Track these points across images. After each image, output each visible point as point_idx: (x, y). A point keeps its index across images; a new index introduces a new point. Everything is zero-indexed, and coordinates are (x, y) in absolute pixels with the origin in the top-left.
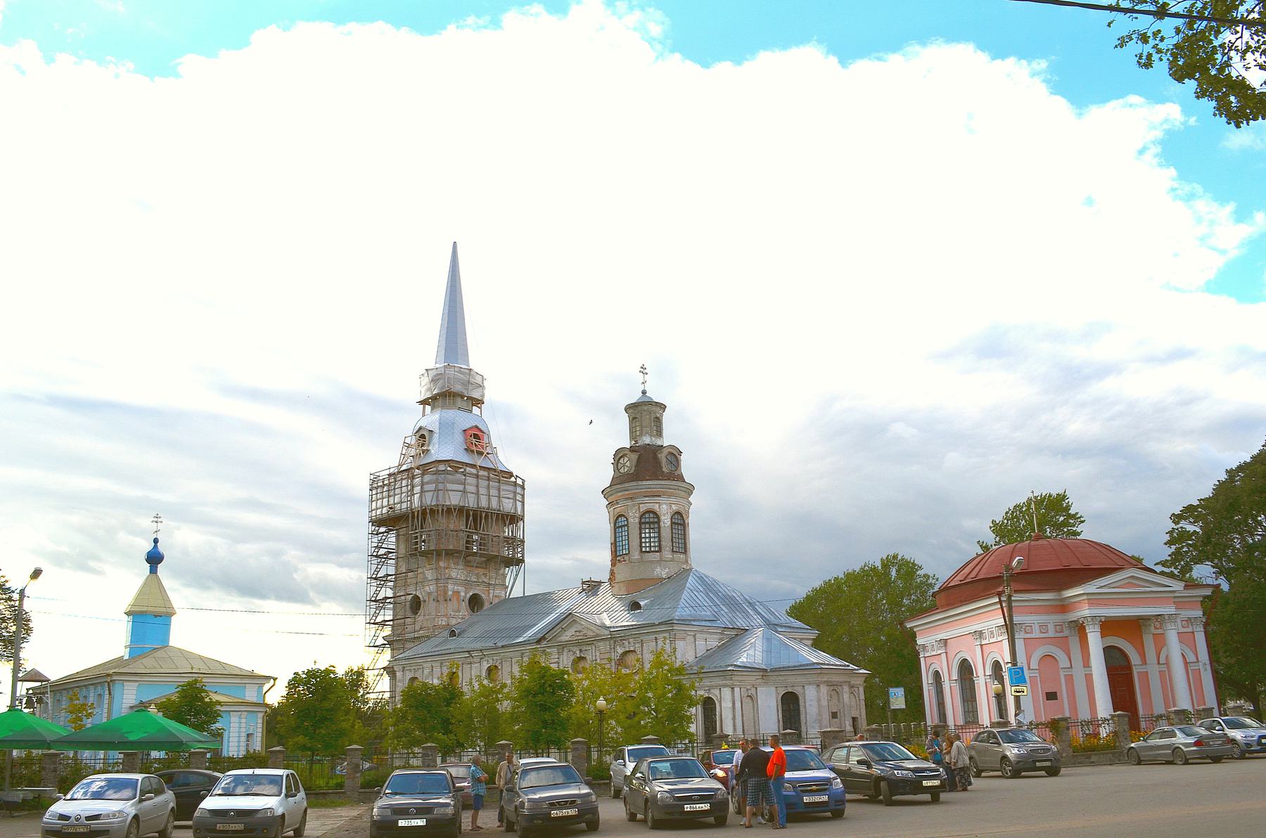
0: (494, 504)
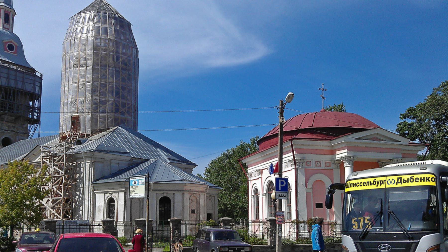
0: (20, 86)
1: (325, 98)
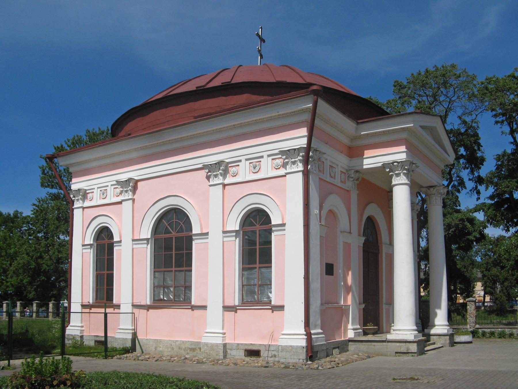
1: (264, 41)
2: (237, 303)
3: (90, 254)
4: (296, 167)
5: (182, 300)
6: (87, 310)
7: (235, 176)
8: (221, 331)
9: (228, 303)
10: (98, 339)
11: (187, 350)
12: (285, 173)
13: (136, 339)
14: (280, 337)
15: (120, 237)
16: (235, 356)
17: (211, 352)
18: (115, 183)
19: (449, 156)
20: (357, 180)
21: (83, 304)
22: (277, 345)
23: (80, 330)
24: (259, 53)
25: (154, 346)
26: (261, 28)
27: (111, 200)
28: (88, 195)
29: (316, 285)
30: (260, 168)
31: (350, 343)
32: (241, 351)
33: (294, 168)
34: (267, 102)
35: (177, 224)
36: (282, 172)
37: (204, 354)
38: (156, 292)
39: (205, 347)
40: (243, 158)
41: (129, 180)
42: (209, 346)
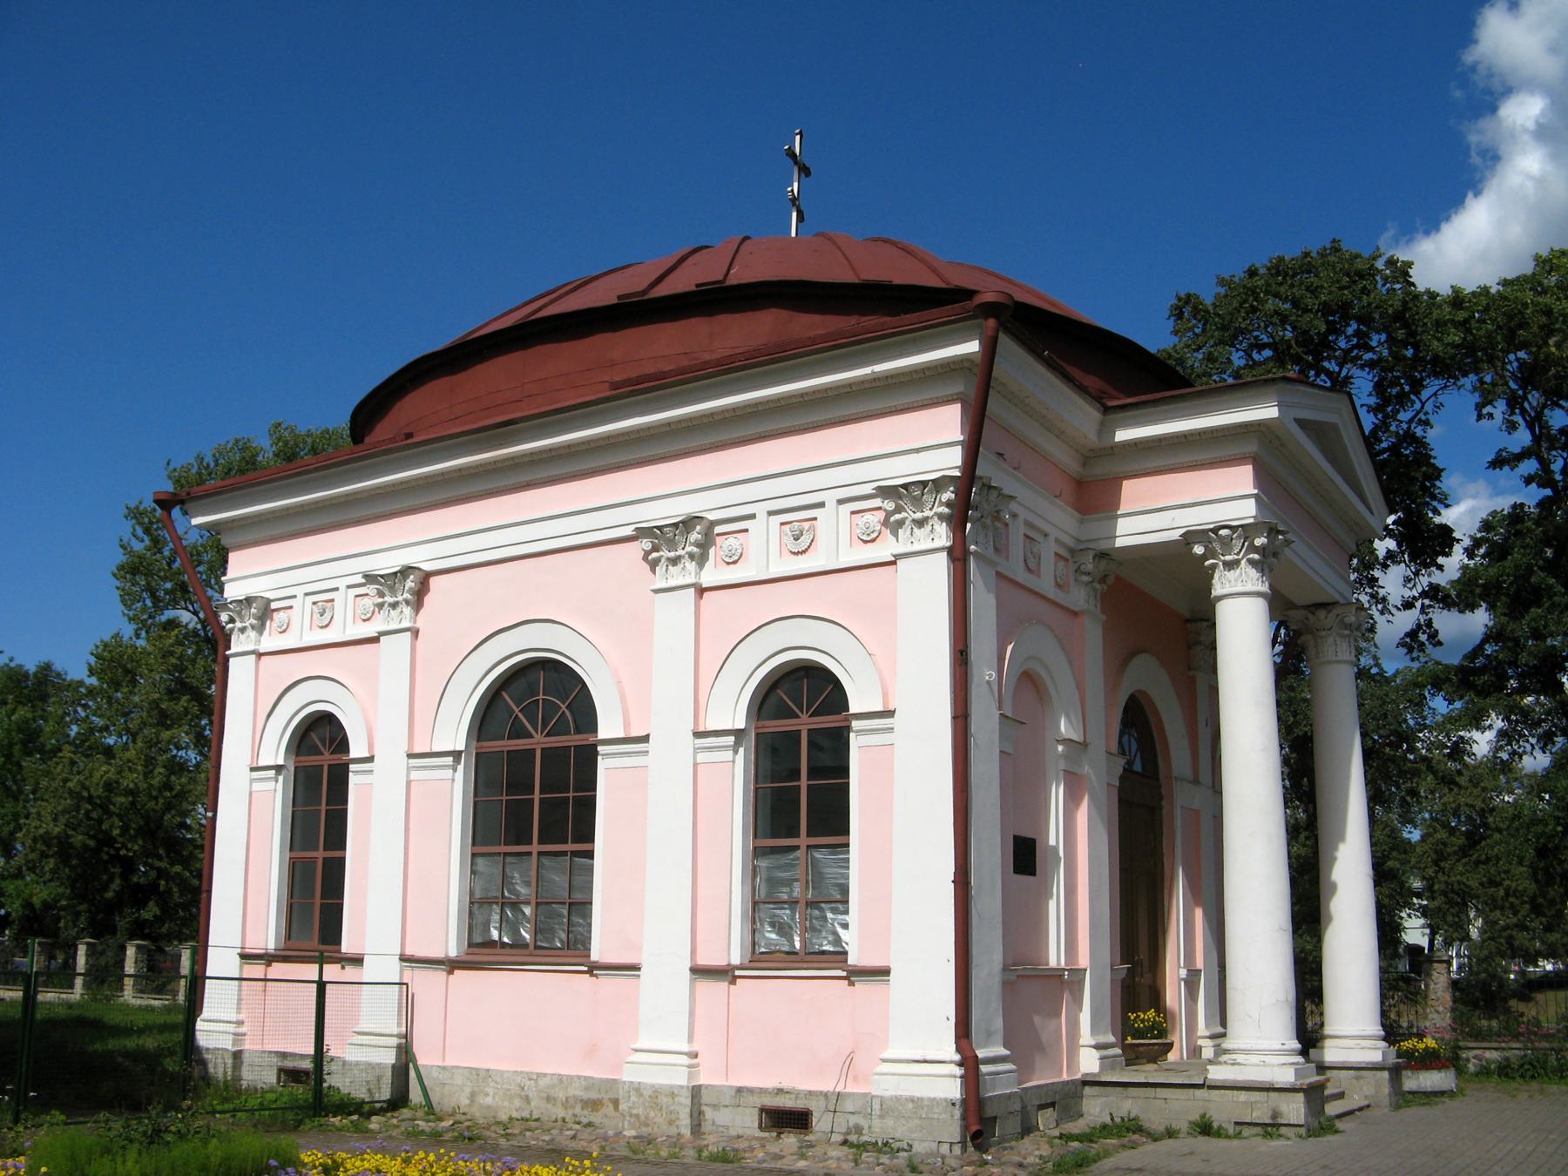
2: (736, 960)
3: (274, 798)
4: (929, 535)
5: (559, 945)
6: (257, 970)
7: (735, 562)
8: (685, 1048)
9: (706, 959)
10: (289, 1064)
11: (573, 1107)
12: (894, 556)
13: (411, 1065)
14: (630, 1059)
15: (371, 746)
16: (727, 1128)
17: (652, 1114)
18: (361, 580)
19: (1372, 513)
20: (1103, 580)
21: (248, 950)
22: (865, 1095)
23: (235, 1034)
24: (794, 204)
25: (468, 1090)
26: (801, 133)
27: (838, 559)
28: (275, 614)
29: (988, 903)
30: (812, 541)
31: (1088, 1090)
32: (748, 1111)
33: (922, 539)
34: (646, 385)
35: (550, 708)
36: (886, 548)
37: (629, 1121)
38: (479, 919)
39: (633, 1098)
40: (760, 509)
41: (406, 571)
42: (645, 1093)
